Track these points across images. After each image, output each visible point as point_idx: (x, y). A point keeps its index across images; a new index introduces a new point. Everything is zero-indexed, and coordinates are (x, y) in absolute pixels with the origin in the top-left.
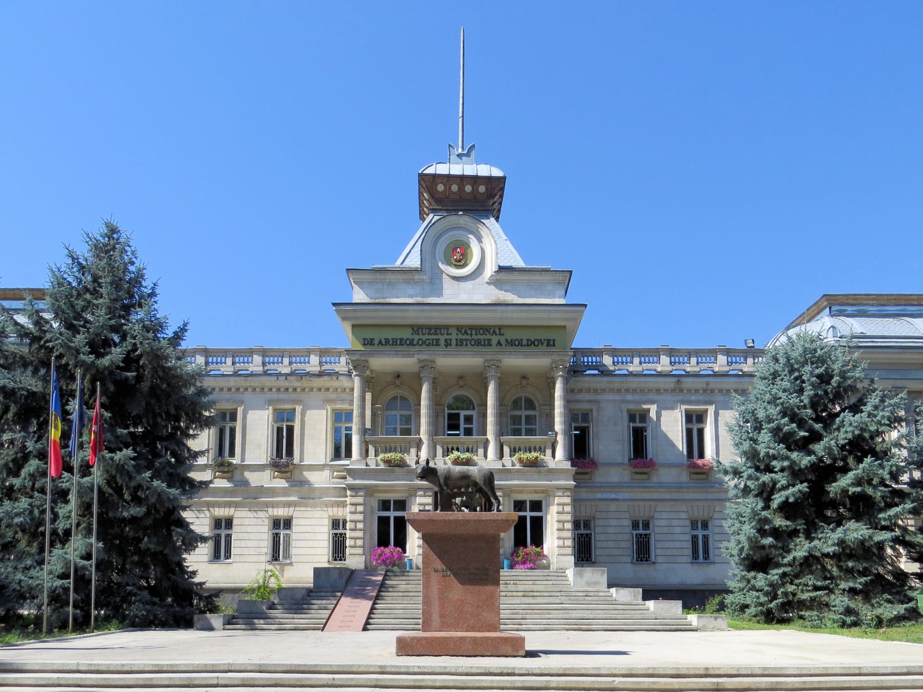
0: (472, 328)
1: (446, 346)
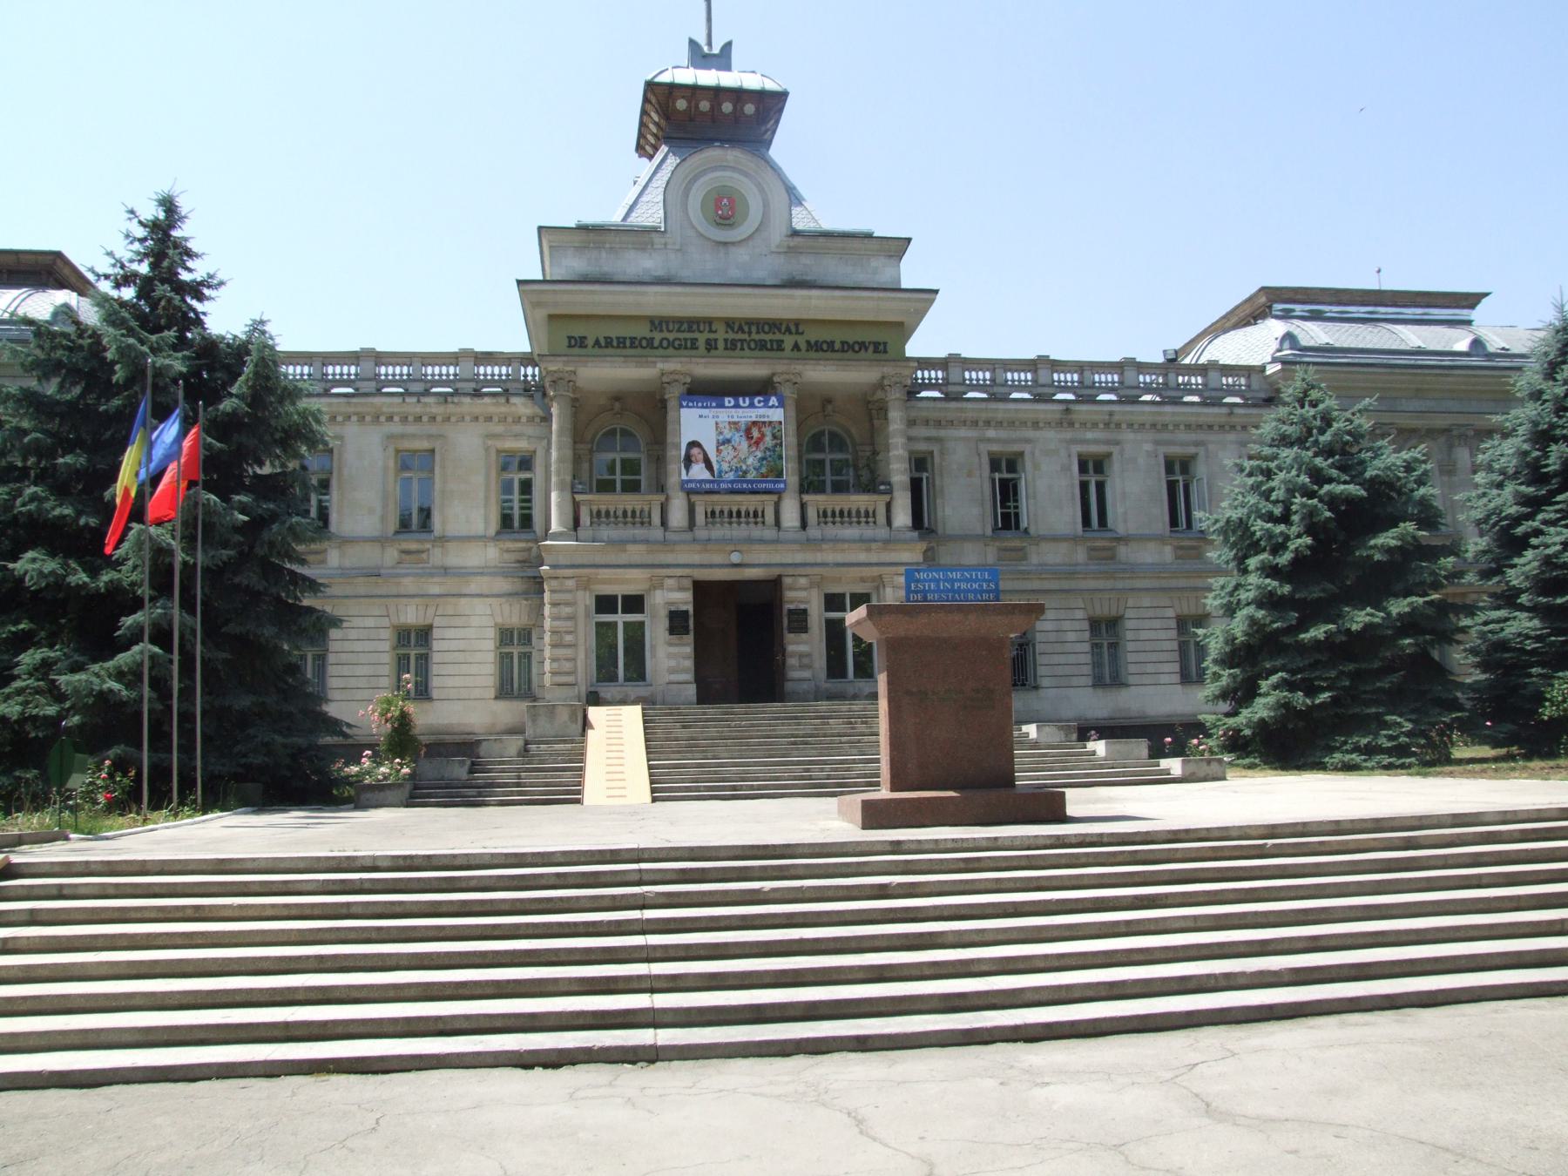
0: (750, 322)
1: (708, 350)
